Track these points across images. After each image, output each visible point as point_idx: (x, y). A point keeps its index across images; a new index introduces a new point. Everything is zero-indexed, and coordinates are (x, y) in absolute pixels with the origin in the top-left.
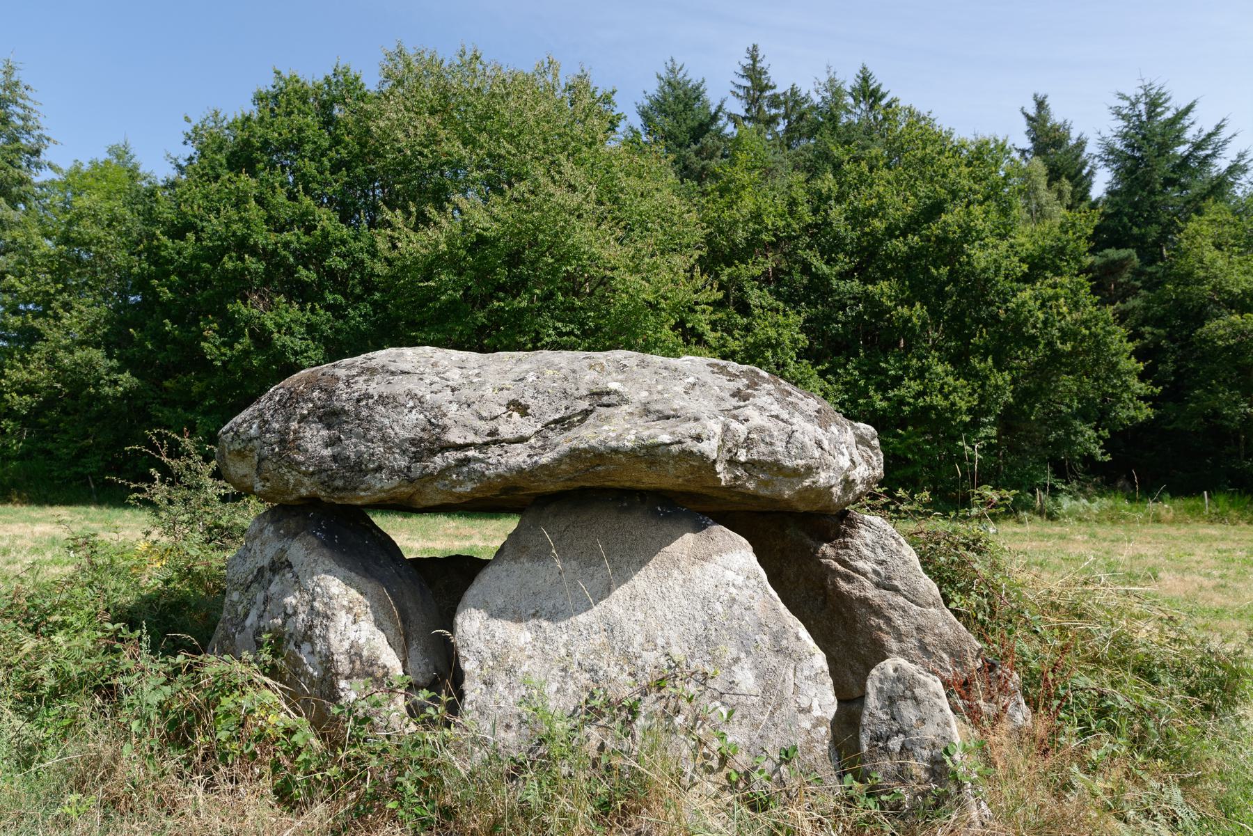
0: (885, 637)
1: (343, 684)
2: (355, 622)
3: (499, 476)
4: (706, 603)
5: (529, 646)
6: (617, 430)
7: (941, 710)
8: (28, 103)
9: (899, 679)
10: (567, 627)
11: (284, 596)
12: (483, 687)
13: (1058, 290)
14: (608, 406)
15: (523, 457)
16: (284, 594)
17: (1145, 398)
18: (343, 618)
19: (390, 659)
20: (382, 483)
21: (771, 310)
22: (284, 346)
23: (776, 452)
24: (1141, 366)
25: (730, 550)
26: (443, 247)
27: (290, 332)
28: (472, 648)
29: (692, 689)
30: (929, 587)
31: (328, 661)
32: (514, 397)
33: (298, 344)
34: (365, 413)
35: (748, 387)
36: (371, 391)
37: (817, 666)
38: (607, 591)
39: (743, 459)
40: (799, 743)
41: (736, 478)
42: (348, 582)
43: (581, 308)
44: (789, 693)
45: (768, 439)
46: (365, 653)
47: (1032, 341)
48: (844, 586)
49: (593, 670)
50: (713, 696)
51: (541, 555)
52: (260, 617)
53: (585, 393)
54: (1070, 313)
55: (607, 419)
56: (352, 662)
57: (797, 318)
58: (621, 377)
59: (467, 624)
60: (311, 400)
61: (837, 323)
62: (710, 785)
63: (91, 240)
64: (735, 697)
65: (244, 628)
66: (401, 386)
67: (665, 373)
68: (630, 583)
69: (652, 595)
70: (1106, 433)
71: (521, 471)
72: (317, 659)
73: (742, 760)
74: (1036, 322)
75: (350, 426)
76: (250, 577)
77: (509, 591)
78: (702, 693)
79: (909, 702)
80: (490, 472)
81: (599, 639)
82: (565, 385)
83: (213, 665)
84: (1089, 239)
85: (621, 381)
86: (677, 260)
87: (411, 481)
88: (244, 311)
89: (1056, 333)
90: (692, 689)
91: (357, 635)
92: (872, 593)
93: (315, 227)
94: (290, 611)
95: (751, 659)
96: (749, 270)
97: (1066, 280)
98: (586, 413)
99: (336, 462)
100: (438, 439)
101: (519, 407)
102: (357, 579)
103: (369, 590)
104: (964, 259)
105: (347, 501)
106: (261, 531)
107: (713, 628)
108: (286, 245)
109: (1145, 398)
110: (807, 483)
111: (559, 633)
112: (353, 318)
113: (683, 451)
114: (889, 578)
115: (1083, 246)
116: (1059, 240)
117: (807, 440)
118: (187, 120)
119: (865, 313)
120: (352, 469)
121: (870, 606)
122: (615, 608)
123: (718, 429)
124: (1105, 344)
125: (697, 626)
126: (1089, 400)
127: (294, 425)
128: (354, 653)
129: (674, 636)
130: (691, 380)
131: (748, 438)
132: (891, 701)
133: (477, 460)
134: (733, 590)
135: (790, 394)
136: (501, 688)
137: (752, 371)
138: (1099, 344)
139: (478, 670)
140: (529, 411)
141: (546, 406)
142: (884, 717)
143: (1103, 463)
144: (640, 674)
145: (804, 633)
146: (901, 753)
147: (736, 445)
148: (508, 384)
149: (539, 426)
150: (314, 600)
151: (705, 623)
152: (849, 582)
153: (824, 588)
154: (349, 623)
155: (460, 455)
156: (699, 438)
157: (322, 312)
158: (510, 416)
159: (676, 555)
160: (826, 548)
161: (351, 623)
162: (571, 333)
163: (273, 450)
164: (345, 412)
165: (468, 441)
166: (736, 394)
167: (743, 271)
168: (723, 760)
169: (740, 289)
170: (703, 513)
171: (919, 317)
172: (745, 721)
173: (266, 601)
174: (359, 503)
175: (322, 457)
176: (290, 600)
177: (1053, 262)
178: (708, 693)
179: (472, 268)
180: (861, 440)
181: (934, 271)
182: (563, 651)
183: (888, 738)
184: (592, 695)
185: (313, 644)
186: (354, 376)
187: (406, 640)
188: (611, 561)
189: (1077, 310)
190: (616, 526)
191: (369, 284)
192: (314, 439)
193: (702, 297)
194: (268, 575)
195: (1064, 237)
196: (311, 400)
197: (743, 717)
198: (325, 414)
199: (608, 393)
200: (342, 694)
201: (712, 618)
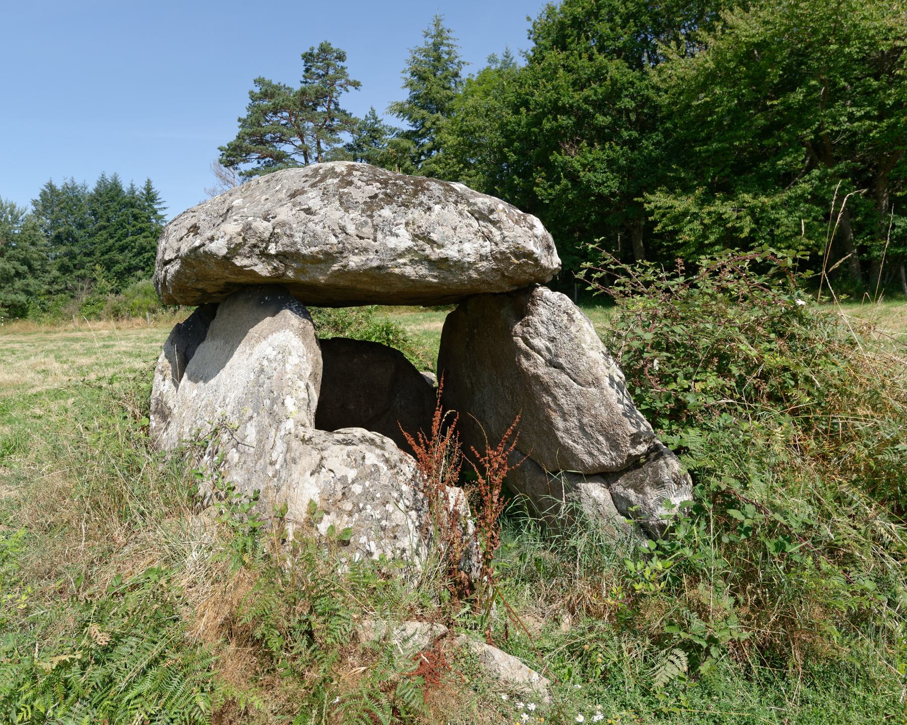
2: (164, 380)
8: (450, 42)
26: (711, 65)
27: (593, 169)
33: (600, 177)
41: (275, 268)
43: (880, 88)
48: (525, 363)
56: (157, 404)
63: (475, 129)
88: (560, 158)
92: (542, 370)
93: (605, 79)
108: (586, 100)
110: (336, 267)
112: (646, 148)
114: (556, 356)
118: (529, 19)
121: (541, 383)
134: (265, 363)
152: (528, 360)
162: (867, 116)
179: (746, 77)
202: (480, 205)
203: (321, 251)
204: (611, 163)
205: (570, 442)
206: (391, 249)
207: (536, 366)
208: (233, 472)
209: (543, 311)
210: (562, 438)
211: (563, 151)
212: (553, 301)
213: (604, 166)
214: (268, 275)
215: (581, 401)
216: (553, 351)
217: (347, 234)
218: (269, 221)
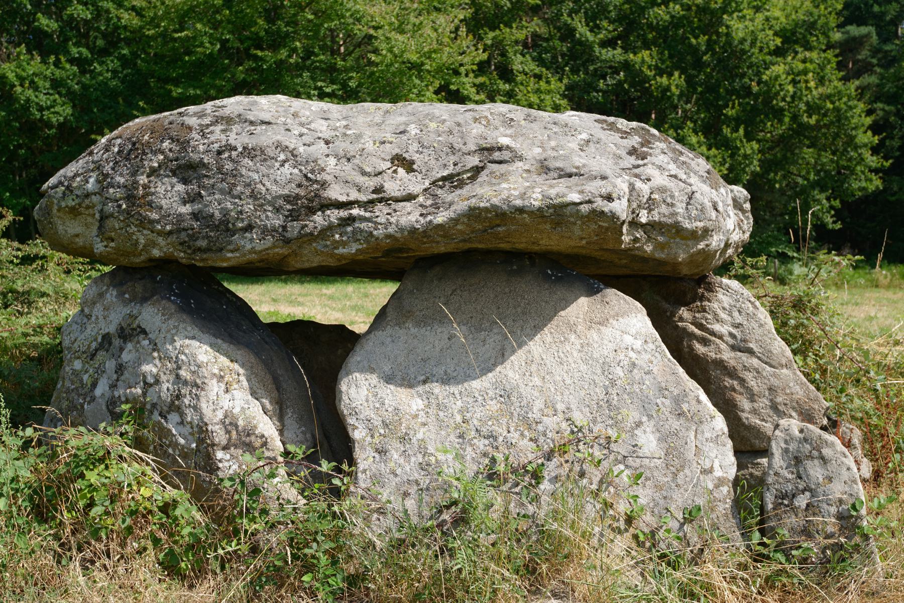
0: (738, 398)
1: (220, 455)
2: (227, 391)
3: (389, 236)
4: (606, 367)
6: (514, 188)
7: (848, 469)
9: (806, 440)
10: (460, 393)
11: (140, 365)
12: (377, 455)
13: (808, 65)
16: (139, 362)
17: (876, 171)
18: (214, 388)
19: (267, 427)
20: (252, 245)
22: (28, 100)
23: (677, 214)
24: (876, 140)
25: (624, 314)
29: (598, 453)
30: (780, 347)
31: (201, 432)
32: (397, 151)
33: (43, 100)
34: (229, 166)
35: (642, 145)
36: (232, 141)
37: (718, 428)
38: (502, 356)
39: (644, 220)
40: (700, 502)
41: (636, 240)
44: (690, 455)
45: (669, 200)
46: (241, 423)
47: (778, 114)
48: (700, 348)
50: (616, 460)
51: (435, 318)
52: (113, 386)
53: (473, 148)
54: (816, 88)
55: (503, 177)
56: (228, 432)
57: (559, 84)
58: (509, 132)
59: (353, 391)
60: (162, 152)
61: (597, 92)
62: (621, 543)
64: (638, 460)
65: (93, 399)
66: (266, 138)
67: (556, 129)
69: (549, 360)
70: (837, 203)
71: (413, 231)
72: (187, 430)
73: (646, 521)
74: (785, 96)
75: (212, 181)
76: (94, 345)
77: (396, 357)
78: (606, 457)
79: (816, 462)
80: (379, 233)
82: (451, 139)
83: (75, 439)
84: (838, 14)
85: (511, 136)
86: (441, 19)
87: (287, 241)
89: (803, 107)
90: (598, 453)
92: (727, 355)
94: (150, 380)
95: (652, 423)
96: (517, 33)
97: (814, 55)
98: (477, 171)
99: (197, 220)
100: (316, 196)
102: (225, 346)
103: (239, 357)
104: (723, 30)
105: (210, 263)
106: (101, 295)
109: (876, 171)
110: (701, 246)
111: (453, 398)
112: (100, 74)
113: (594, 211)
114: (745, 341)
115: (833, 21)
116: (811, 14)
119: (625, 81)
120: (216, 228)
121: (725, 368)
122: (511, 374)
123: (625, 187)
124: (847, 118)
125: (597, 390)
126: (826, 172)
127: (143, 179)
128: (229, 423)
130: (584, 136)
131: (650, 198)
134: (632, 355)
135: (681, 153)
136: (396, 456)
137: (643, 129)
138: (840, 117)
139: (369, 439)
140: (415, 167)
141: (433, 162)
142: (790, 476)
143: (833, 231)
144: (542, 439)
145: (704, 397)
147: (639, 206)
148: (389, 137)
150: (179, 368)
151: (606, 387)
152: (705, 345)
154: (221, 393)
155: (343, 213)
156: (609, 198)
157: (68, 66)
158: (395, 172)
159: (573, 320)
160: (684, 312)
161: (226, 393)
163: (120, 206)
164: (204, 165)
165: (352, 198)
166: (633, 152)
167: (507, 36)
168: (629, 520)
169: (503, 54)
170: (594, 277)
171: (677, 86)
172: (648, 483)
173: (120, 369)
174: (225, 265)
175: (180, 215)
176: (149, 368)
177: (804, 37)
178: (612, 457)
181: (693, 41)
182: (459, 418)
183: (794, 496)
184: (493, 460)
185: (182, 414)
186: (208, 126)
187: (281, 409)
189: (823, 85)
190: (507, 290)
191: (113, 38)
192: (169, 195)
193: (466, 59)
194: (117, 342)
195: (815, 11)
196: (162, 152)
198: (179, 167)
200: (220, 465)
201: (613, 383)
204: (56, 84)
205: (758, 421)
207: (720, 351)
210: (747, 418)
212: (735, 288)
213: (48, 85)
215: (775, 382)
216: (739, 337)
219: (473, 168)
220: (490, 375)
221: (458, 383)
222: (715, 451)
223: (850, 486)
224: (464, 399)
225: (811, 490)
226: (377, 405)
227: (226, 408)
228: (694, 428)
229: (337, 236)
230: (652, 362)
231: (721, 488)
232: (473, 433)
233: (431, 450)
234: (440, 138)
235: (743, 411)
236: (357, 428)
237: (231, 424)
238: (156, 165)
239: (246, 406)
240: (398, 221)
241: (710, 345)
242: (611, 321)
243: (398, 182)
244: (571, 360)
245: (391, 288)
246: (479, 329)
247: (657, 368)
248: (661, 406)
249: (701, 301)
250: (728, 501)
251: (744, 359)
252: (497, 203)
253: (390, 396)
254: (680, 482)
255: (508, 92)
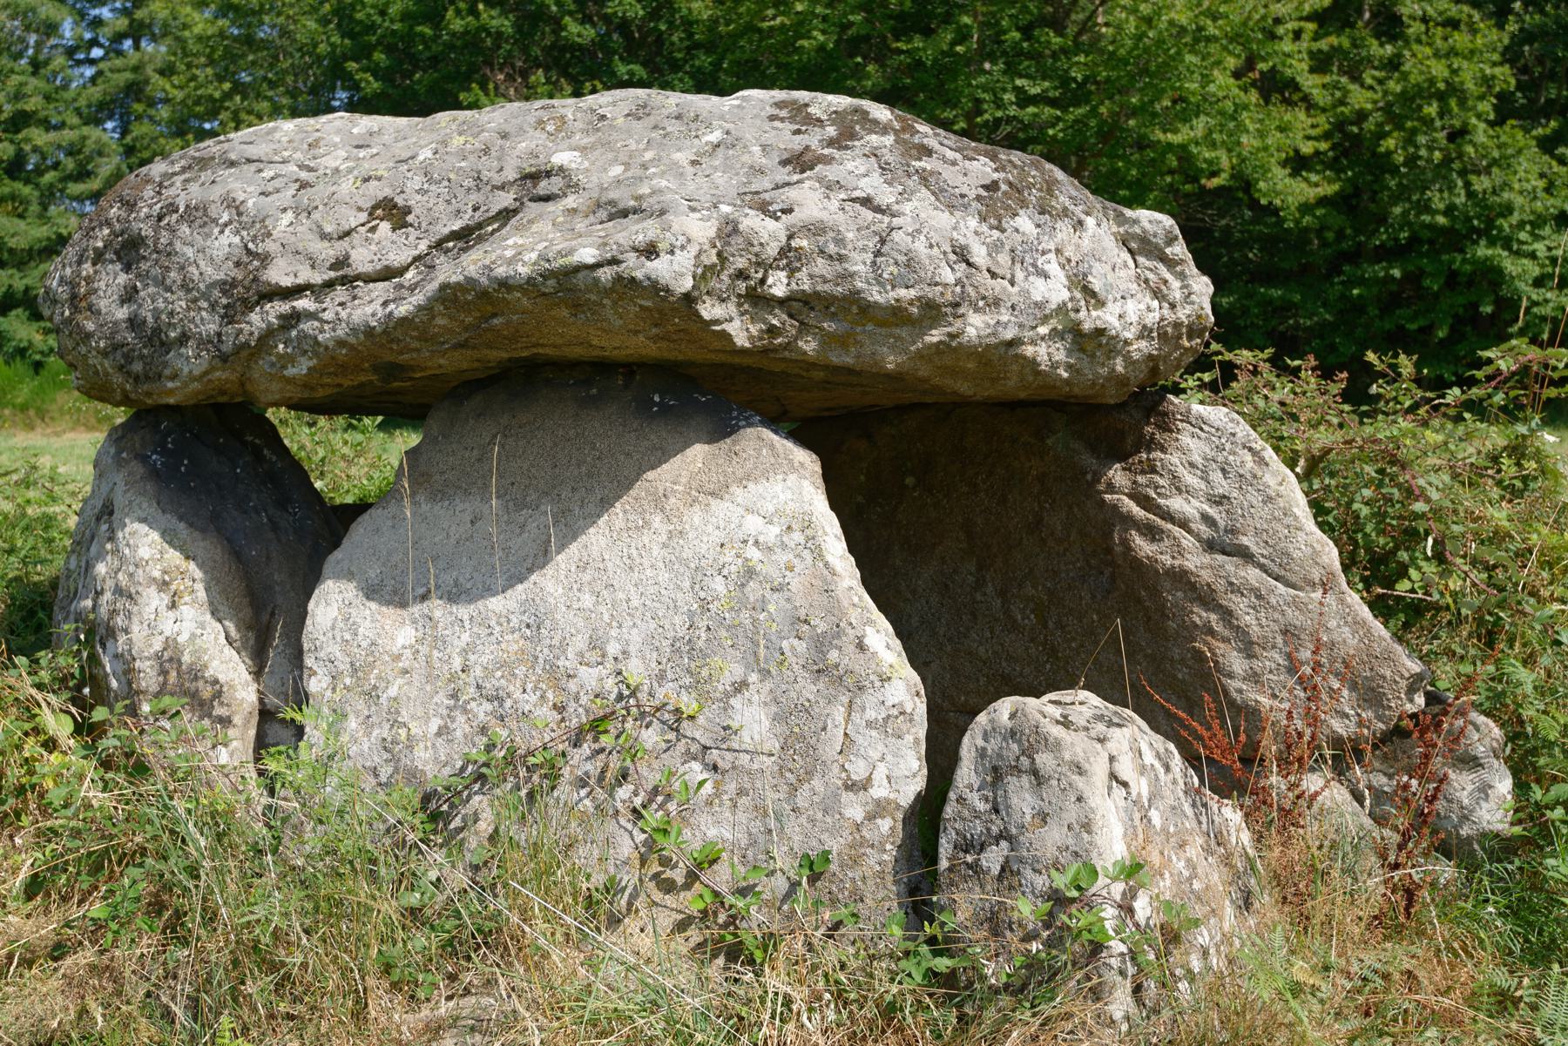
0: (1221, 648)
2: (173, 606)
3: (341, 343)
4: (699, 575)
5: (408, 653)
9: (1013, 733)
14: (547, 199)
15: (376, 306)
18: (153, 600)
21: (1444, 25)
23: (852, 275)
28: (322, 654)
32: (388, 192)
38: (541, 557)
39: (779, 291)
40: (835, 845)
41: (772, 331)
42: (170, 537)
45: (832, 249)
46: (186, 659)
48: (1143, 547)
49: (497, 698)
56: (164, 673)
57: (1494, 35)
64: (729, 756)
68: (583, 539)
71: (369, 331)
77: (389, 554)
81: (513, 644)
91: (176, 628)
92: (1195, 561)
95: (768, 685)
101: (393, 212)
107: (703, 624)
110: (935, 336)
113: (619, 278)
114: (1233, 531)
117: (920, 246)
121: (1193, 587)
122: (550, 586)
125: (677, 620)
127: (87, 268)
128: (169, 659)
129: (636, 637)
132: (996, 775)
133: (312, 316)
134: (753, 553)
135: (929, 152)
139: (329, 693)
141: (442, 206)
142: (982, 806)
144: (572, 706)
146: (1000, 878)
149: (423, 247)
152: (1153, 540)
153: (1109, 550)
156: (650, 251)
160: (1117, 474)
165: (300, 281)
172: (743, 801)
175: (115, 323)
178: (681, 747)
180: (1140, 246)
182: (457, 663)
183: (982, 847)
188: (415, 503)
190: (572, 433)
196: (108, 223)
197: (741, 792)
199: (548, 174)
201: (705, 606)
202: (1147, 226)
203: (919, 299)
206: (1036, 304)
207: (1180, 551)
208: (703, 819)
209: (1192, 444)
210: (1240, 691)
211: (491, 86)
212: (1217, 423)
214: (747, 345)
216: (1221, 524)
217: (969, 264)
218: (777, 219)
219: (500, 212)
220: (520, 587)
221: (470, 602)
222: (881, 747)
223: (1078, 835)
224: (475, 629)
225: (1010, 839)
226: (347, 636)
227: (167, 633)
228: (845, 700)
229: (281, 346)
230: (791, 569)
231: (879, 821)
232: (472, 690)
233: (404, 716)
234: (463, 164)
235: (1231, 676)
236: (315, 673)
237: (171, 660)
238: (100, 244)
239: (199, 632)
240: (350, 315)
241: (1161, 540)
242: (733, 488)
243: (373, 247)
244: (646, 563)
245: (413, 439)
246: (521, 505)
247: (802, 578)
248: (788, 653)
249: (1149, 451)
250: (888, 847)
251: (1230, 568)
252: (476, 276)
253: (368, 623)
254: (801, 802)
255: (1390, 61)
